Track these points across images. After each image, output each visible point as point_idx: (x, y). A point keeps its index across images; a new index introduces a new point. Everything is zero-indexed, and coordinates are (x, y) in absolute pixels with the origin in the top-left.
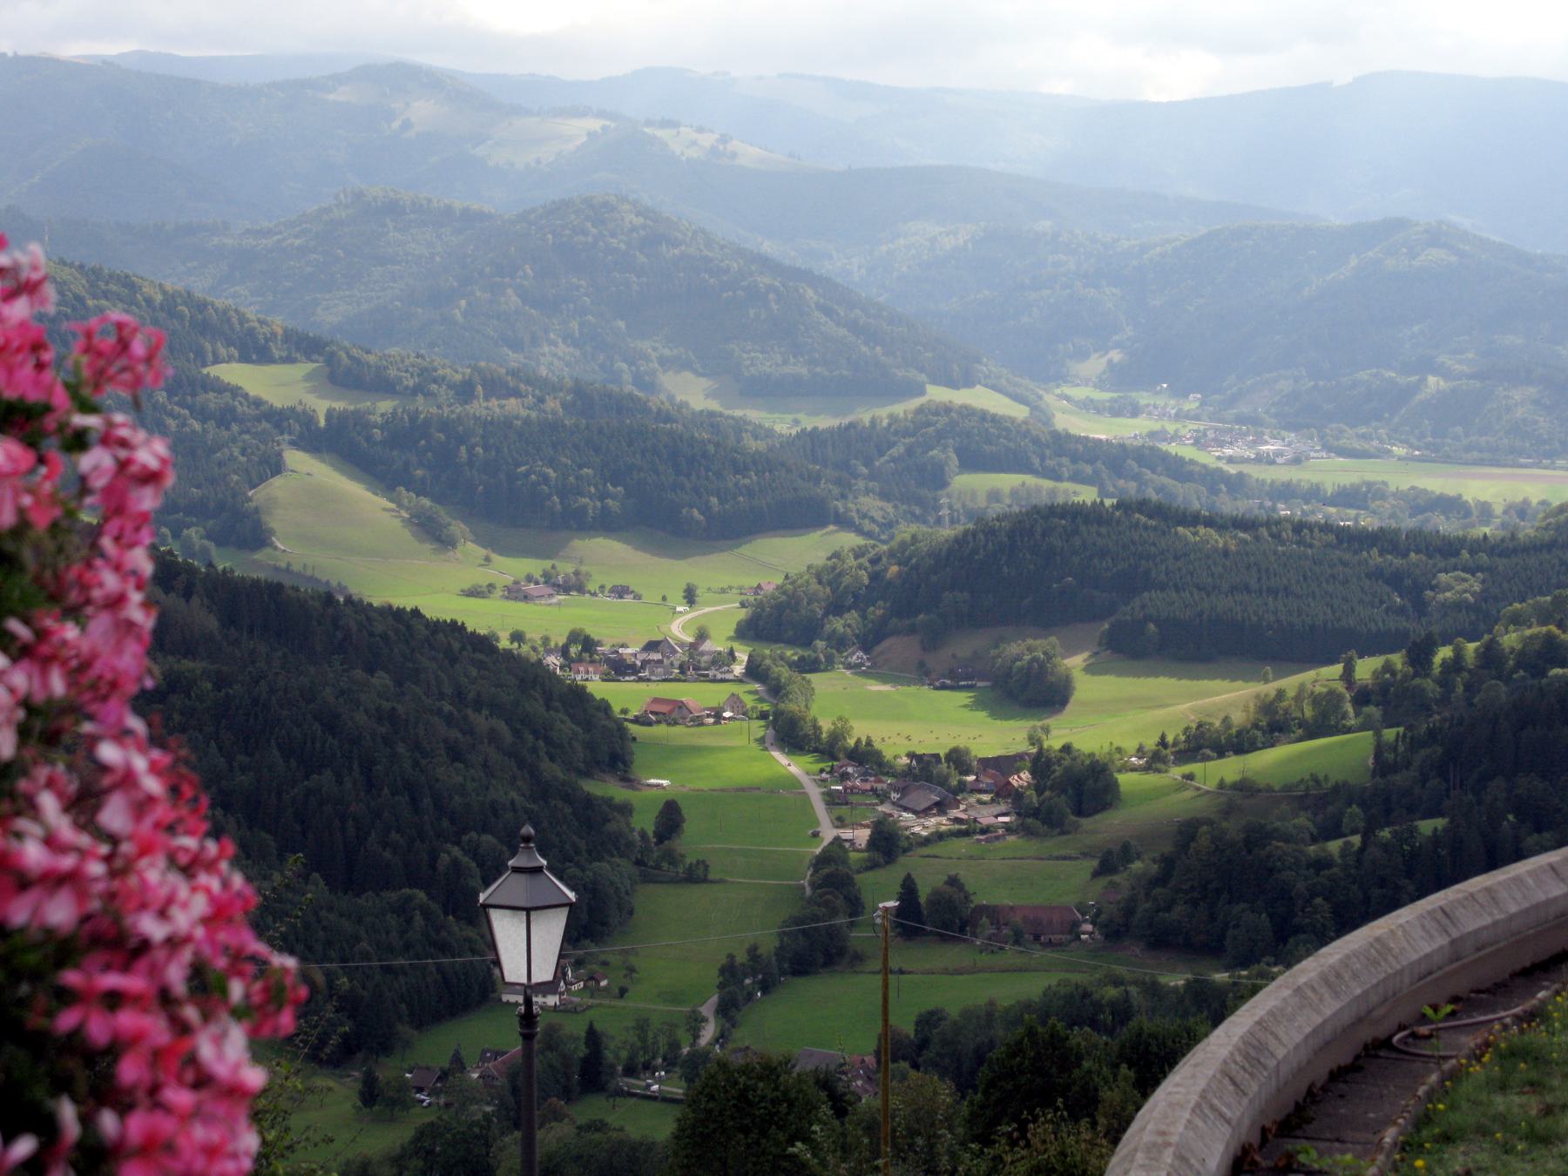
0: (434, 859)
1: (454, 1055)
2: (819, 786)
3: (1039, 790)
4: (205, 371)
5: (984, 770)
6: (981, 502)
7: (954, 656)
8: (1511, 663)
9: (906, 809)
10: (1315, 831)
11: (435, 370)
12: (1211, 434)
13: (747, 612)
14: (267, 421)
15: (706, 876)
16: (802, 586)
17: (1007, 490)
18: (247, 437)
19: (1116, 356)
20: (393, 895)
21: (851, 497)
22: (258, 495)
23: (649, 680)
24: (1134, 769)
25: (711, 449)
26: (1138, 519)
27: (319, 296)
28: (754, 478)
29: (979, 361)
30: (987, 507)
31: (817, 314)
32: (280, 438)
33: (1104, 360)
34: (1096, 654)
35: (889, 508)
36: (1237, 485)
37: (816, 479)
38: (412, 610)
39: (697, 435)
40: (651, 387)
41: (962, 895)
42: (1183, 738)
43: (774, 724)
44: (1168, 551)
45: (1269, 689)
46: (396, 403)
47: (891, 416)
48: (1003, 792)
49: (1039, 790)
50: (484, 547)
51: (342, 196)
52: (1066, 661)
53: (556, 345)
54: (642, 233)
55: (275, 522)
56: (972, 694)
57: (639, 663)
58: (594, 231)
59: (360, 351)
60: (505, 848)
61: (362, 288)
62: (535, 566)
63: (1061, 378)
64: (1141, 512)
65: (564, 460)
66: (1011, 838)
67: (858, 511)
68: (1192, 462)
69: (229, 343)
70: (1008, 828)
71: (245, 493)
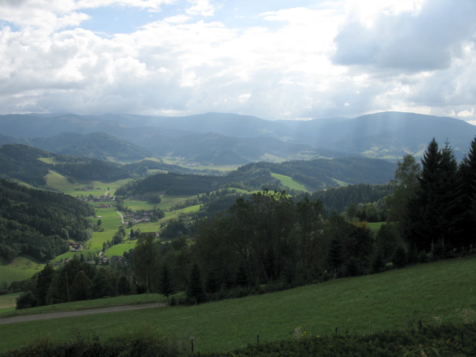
0: (60, 230)
3: (154, 215)
4: (37, 159)
8: (220, 194)
9: (135, 219)
10: (191, 219)
12: (185, 163)
17: (155, 172)
19: (173, 152)
22: (45, 177)
24: (168, 211)
36: (188, 170)
40: (105, 159)
42: (175, 207)
45: (187, 199)
48: (149, 216)
53: (91, 153)
68: (182, 167)
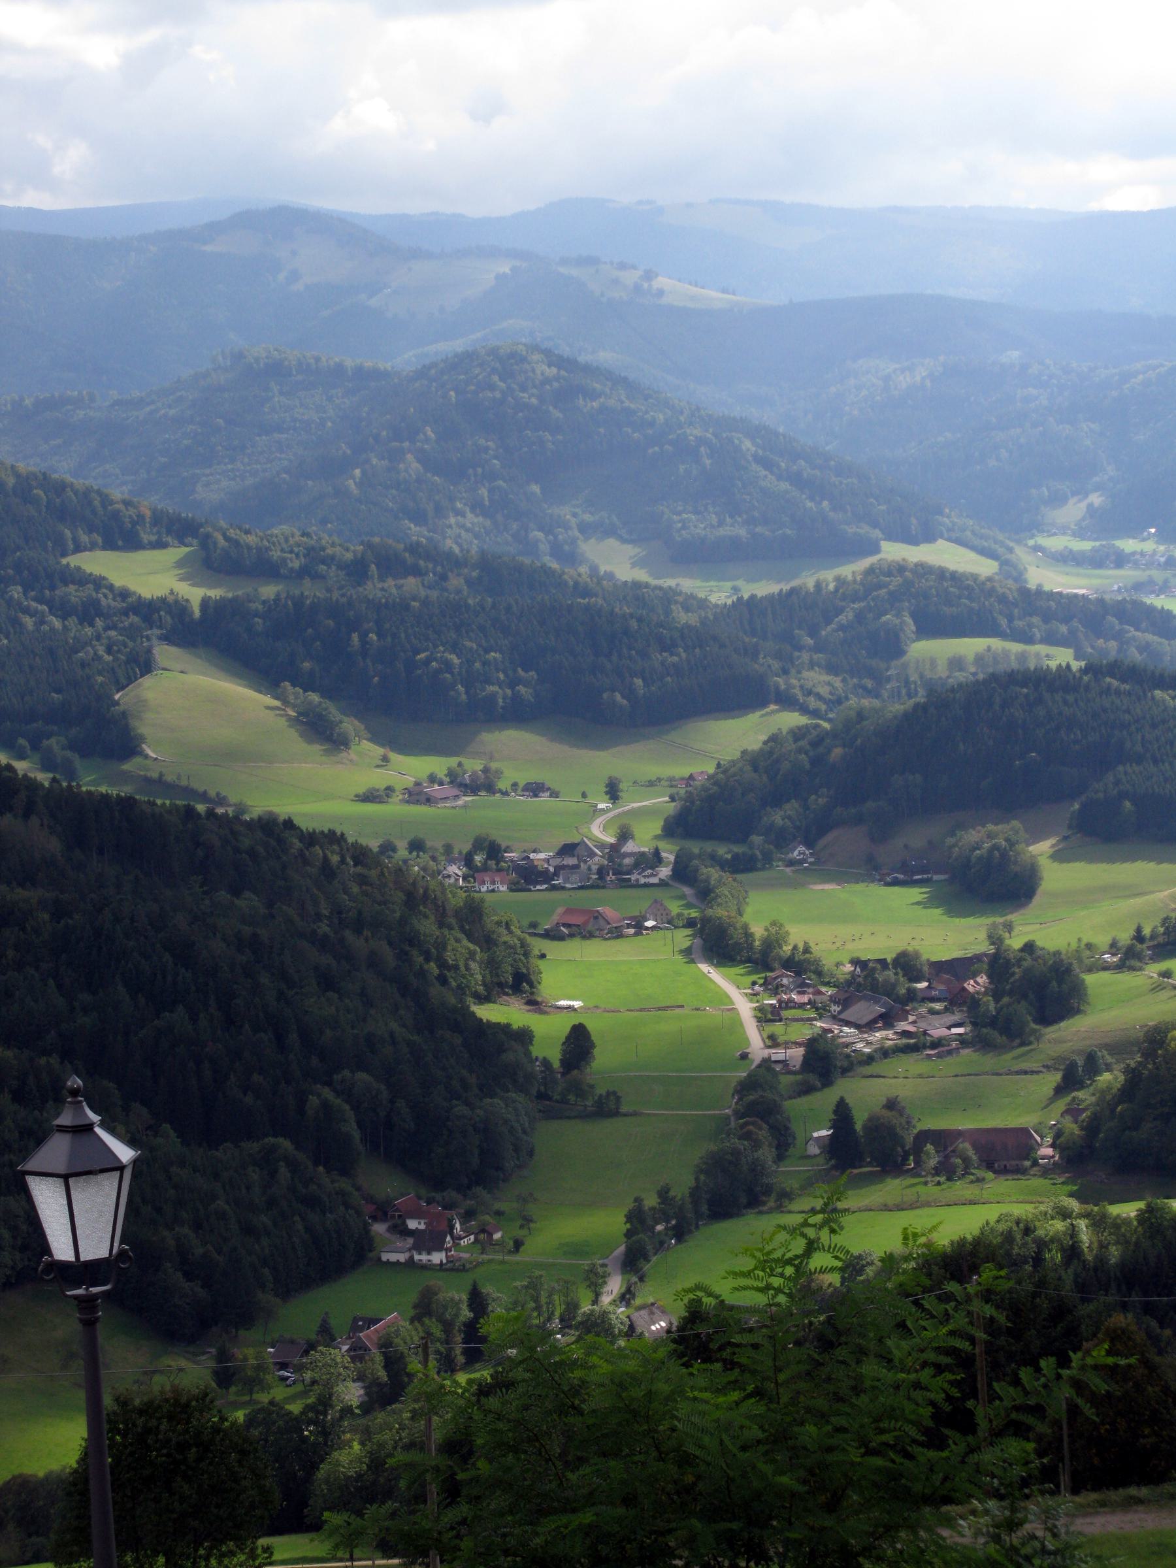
1: (322, 1326)
2: (751, 1001)
3: (997, 995)
4: (64, 561)
5: (937, 975)
6: (942, 671)
7: (906, 846)
9: (848, 1023)
11: (323, 549)
13: (675, 806)
14: (135, 614)
15: (618, 1108)
16: (734, 775)
17: (971, 657)
18: (113, 633)
19: (1096, 499)
20: (255, 1144)
21: (793, 671)
23: (563, 888)
24: (1106, 967)
25: (634, 624)
26: (1109, 684)
27: (198, 471)
28: (684, 655)
29: (941, 513)
30: (948, 677)
31: (754, 466)
32: (149, 632)
33: (1083, 505)
34: (1065, 838)
35: (837, 682)
37: (754, 654)
38: (285, 821)
39: (617, 610)
40: (571, 558)
41: (903, 1120)
42: (1162, 930)
43: (701, 933)
44: (1144, 718)
46: (280, 587)
47: (837, 579)
48: (957, 1000)
49: (997, 996)
50: (382, 745)
51: (220, 359)
52: (1031, 848)
53: (464, 516)
54: (556, 385)
55: (144, 727)
56: (924, 890)
57: (552, 869)
58: (502, 385)
59: (238, 532)
60: (383, 1087)
61: (246, 460)
62: (438, 765)
63: (1037, 527)
64: (1113, 676)
65: (468, 644)
66: (966, 1052)
67: (801, 687)
69: (91, 529)
70: (963, 1041)
71: (110, 697)
